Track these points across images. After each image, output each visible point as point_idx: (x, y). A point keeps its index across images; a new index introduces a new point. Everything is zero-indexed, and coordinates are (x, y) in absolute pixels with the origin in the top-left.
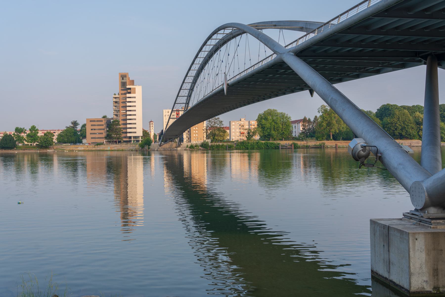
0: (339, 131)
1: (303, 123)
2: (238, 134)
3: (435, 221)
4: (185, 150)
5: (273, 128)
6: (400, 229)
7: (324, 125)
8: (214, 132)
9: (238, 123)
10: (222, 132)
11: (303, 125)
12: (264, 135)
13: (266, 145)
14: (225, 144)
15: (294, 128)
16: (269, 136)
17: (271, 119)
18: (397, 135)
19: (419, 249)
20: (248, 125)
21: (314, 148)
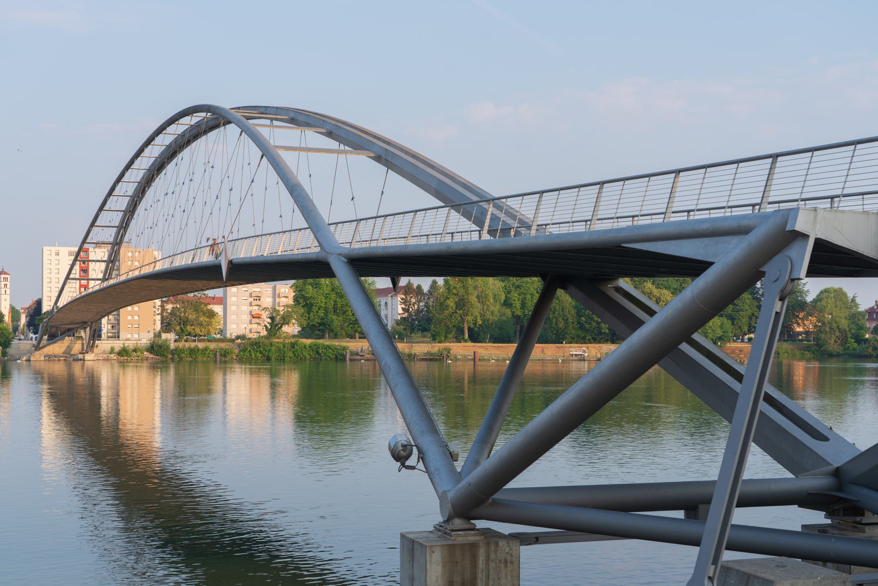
0: (484, 321)
1: (404, 297)
2: (246, 317)
3: (455, 533)
4: (107, 360)
5: (333, 308)
6: (421, 542)
7: (450, 305)
8: (185, 314)
9: (246, 289)
10: (204, 314)
11: (404, 302)
12: (311, 323)
13: (313, 350)
14: (212, 346)
15: (383, 307)
16: (321, 327)
17: (327, 286)
18: (604, 333)
19: (436, 562)
20: (271, 295)
21: (426, 360)
